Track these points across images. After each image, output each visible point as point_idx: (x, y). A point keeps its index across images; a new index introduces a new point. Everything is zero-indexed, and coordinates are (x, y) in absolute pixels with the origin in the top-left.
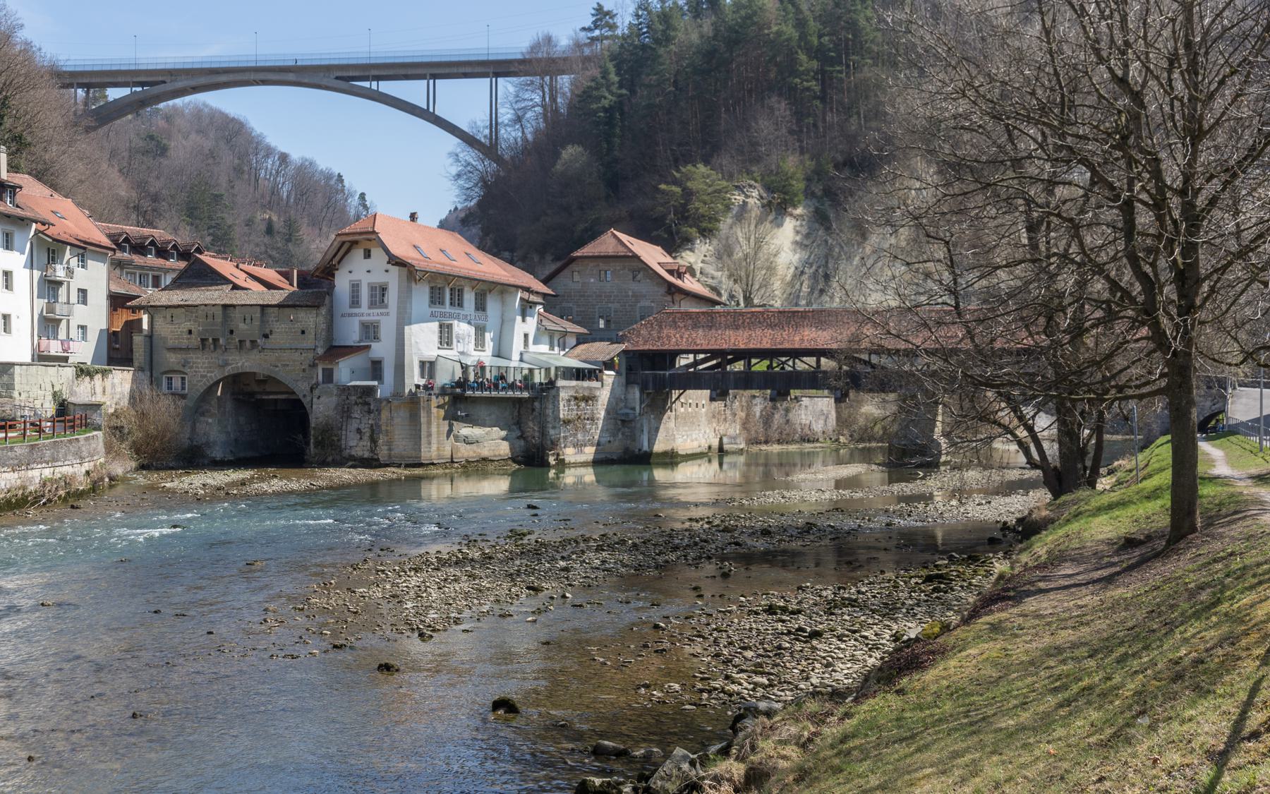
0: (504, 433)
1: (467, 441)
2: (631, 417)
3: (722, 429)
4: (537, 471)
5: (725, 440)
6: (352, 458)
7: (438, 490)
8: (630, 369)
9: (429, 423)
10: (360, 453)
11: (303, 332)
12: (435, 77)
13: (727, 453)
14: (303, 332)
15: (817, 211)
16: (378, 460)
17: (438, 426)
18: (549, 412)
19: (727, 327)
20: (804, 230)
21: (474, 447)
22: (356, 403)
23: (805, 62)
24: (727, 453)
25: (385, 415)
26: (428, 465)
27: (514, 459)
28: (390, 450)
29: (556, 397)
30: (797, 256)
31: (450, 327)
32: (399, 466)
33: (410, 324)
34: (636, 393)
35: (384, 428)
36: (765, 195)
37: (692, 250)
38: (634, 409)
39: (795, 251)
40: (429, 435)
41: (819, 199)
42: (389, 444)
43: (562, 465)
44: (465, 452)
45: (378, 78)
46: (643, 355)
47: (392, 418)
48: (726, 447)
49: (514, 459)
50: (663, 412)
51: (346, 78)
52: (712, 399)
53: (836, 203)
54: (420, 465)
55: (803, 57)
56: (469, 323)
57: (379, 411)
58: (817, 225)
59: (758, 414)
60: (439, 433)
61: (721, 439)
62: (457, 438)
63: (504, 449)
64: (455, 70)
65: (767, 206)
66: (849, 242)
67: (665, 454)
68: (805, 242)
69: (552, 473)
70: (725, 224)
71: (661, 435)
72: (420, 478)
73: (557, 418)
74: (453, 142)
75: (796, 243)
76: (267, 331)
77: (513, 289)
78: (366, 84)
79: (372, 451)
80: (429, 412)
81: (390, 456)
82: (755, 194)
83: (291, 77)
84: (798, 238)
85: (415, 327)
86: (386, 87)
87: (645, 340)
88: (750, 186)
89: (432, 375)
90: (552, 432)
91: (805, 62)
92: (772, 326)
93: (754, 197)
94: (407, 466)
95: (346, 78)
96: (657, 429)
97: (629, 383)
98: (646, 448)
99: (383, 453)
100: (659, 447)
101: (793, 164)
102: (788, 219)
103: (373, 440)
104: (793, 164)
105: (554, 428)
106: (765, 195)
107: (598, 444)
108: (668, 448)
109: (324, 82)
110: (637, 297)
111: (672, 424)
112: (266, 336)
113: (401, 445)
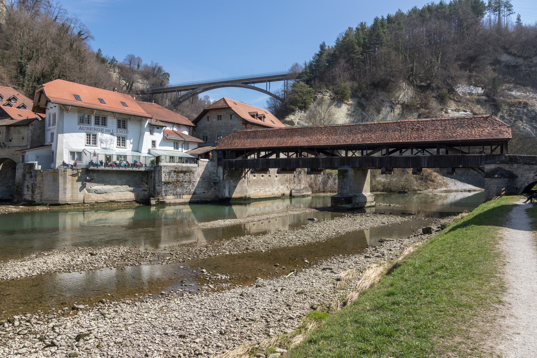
0: (132, 189)
1: (96, 192)
2: (218, 181)
3: (292, 186)
4: (148, 207)
5: (293, 191)
6: (25, 200)
7: (72, 219)
8: (219, 159)
9: (65, 183)
10: (28, 198)
11: (23, 138)
12: (269, 81)
13: (294, 197)
14: (23, 138)
15: (358, 102)
16: (35, 201)
17: (72, 184)
18: (157, 178)
19: (261, 137)
20: (352, 110)
21: (104, 195)
22: (28, 173)
23: (358, 49)
24: (294, 197)
25: (39, 178)
26: (63, 204)
27: (136, 201)
28: (41, 196)
29: (160, 171)
30: (348, 119)
31: (95, 136)
32: (45, 205)
33: (62, 133)
34: (221, 170)
35: (38, 185)
36: (332, 95)
37: (294, 115)
38: (219, 177)
39: (347, 118)
40: (65, 189)
41: (360, 98)
42: (41, 194)
43: (162, 204)
44: (94, 198)
45: (254, 83)
46: (224, 152)
47: (43, 180)
48: (293, 194)
49: (136, 201)
50: (240, 178)
51: (246, 83)
52: (278, 173)
53: (367, 99)
54: (59, 205)
55: (357, 47)
56: (112, 134)
57: (36, 176)
58: (358, 108)
59: (320, 180)
60: (73, 188)
61: (291, 191)
62: (89, 191)
63: (131, 196)
64: (274, 78)
65: (333, 99)
66: (372, 114)
67: (240, 199)
68: (353, 114)
69: (153, 209)
70: (312, 106)
71: (238, 188)
72: (58, 212)
73: (160, 181)
74: (268, 97)
75: (348, 114)
76: (11, 138)
77: (144, 119)
78: (252, 85)
79: (32, 197)
80: (65, 177)
81: (41, 200)
82: (328, 94)
83: (230, 84)
84: (349, 112)
85: (66, 135)
86: (256, 85)
87: (226, 144)
88: (326, 91)
89: (80, 159)
90: (158, 188)
91: (358, 49)
92: (281, 136)
93: (327, 96)
94: (51, 205)
95: (246, 83)
96: (235, 187)
97: (219, 165)
98: (227, 195)
99: (37, 198)
100: (235, 195)
101: (347, 85)
102: (344, 105)
103: (33, 192)
104: (347, 85)
105: (159, 186)
106: (332, 95)
107: (194, 193)
108: (243, 195)
109: (239, 85)
110: (232, 126)
111: (246, 185)
112: (10, 141)
113: (48, 194)
